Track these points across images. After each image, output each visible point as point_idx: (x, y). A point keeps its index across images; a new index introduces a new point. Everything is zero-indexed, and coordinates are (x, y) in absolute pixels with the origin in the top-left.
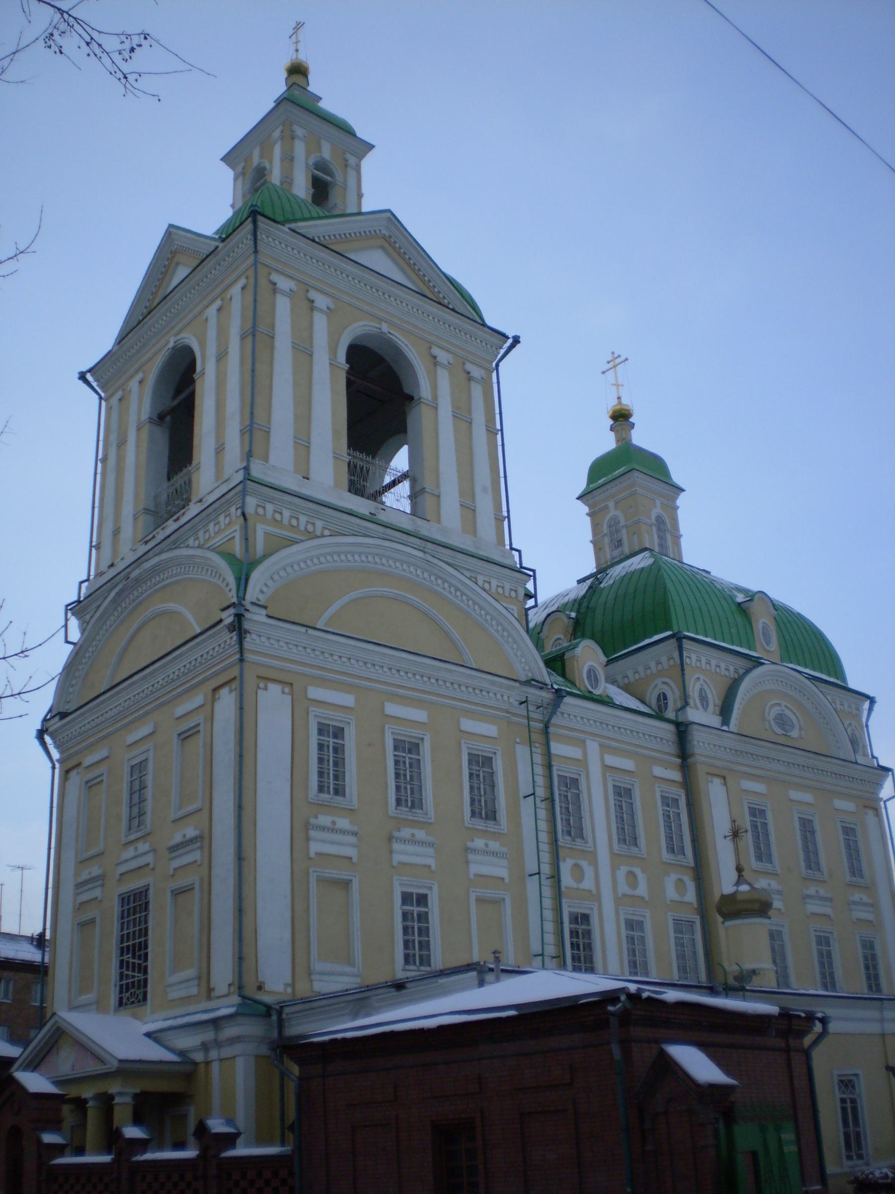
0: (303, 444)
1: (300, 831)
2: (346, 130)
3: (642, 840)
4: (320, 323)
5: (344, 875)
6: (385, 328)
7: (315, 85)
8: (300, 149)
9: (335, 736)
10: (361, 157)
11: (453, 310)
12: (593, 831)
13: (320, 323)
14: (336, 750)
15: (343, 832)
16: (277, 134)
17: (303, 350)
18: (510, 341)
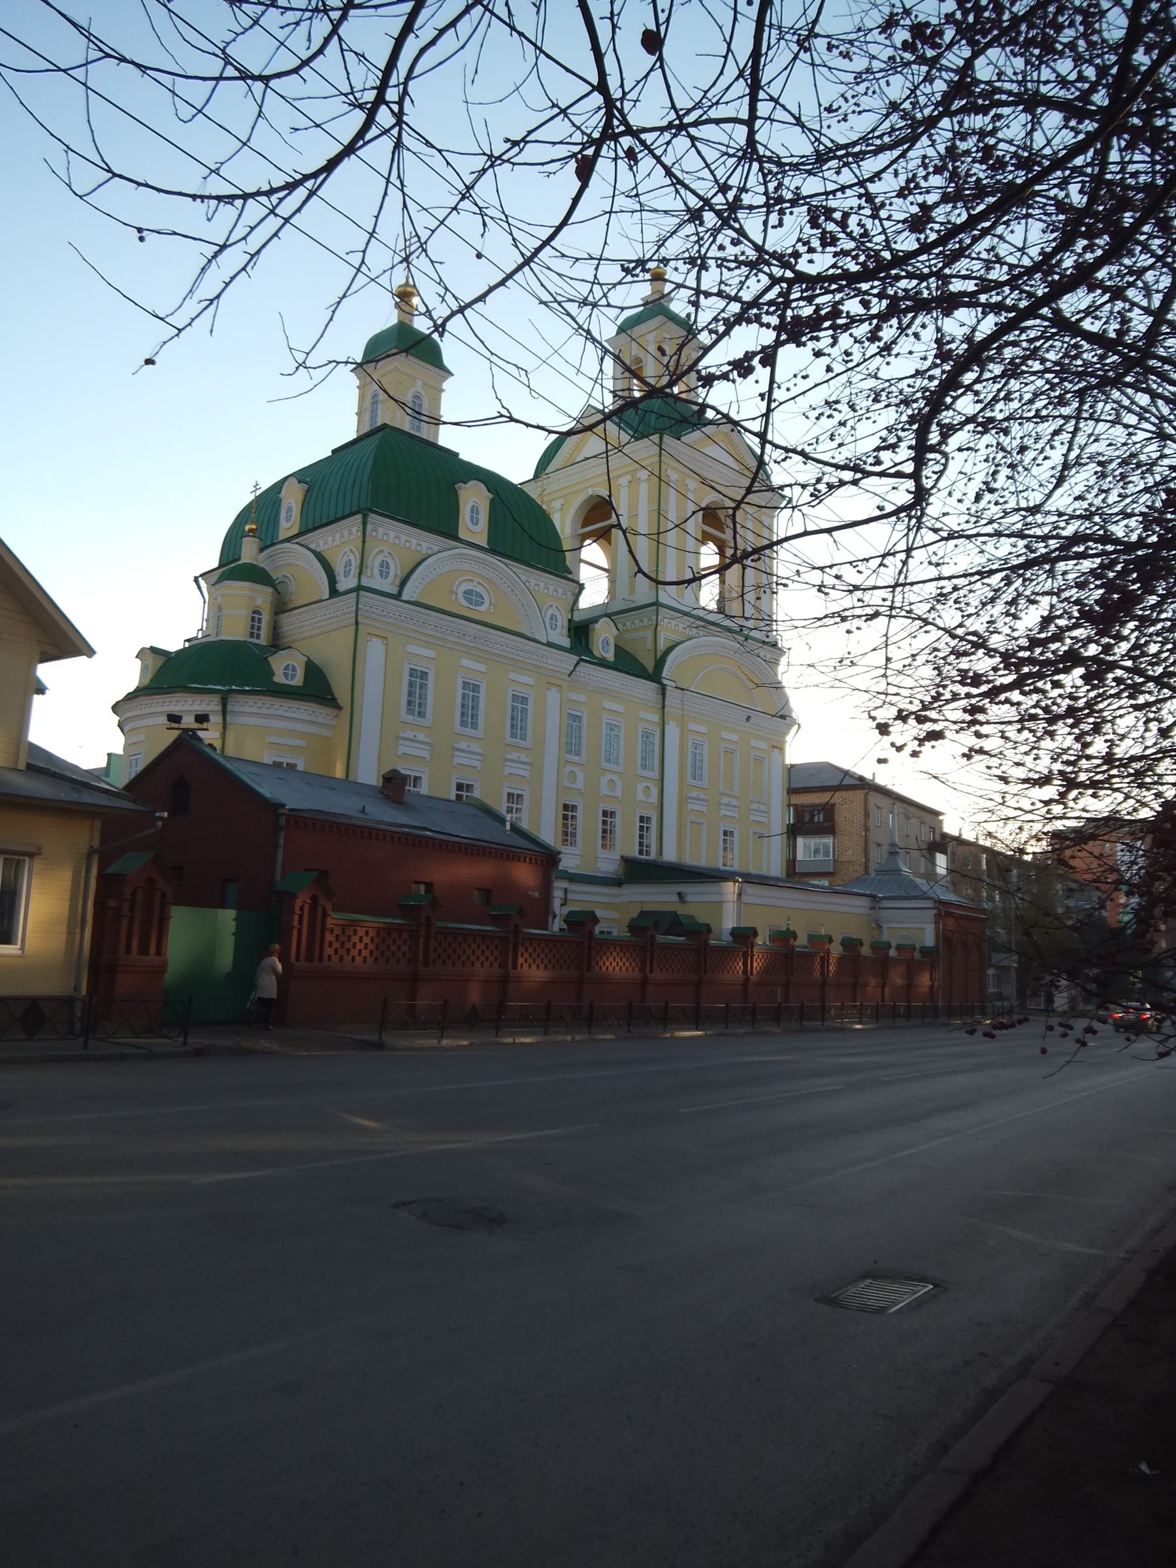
1: (683, 799)
15: (472, 753)
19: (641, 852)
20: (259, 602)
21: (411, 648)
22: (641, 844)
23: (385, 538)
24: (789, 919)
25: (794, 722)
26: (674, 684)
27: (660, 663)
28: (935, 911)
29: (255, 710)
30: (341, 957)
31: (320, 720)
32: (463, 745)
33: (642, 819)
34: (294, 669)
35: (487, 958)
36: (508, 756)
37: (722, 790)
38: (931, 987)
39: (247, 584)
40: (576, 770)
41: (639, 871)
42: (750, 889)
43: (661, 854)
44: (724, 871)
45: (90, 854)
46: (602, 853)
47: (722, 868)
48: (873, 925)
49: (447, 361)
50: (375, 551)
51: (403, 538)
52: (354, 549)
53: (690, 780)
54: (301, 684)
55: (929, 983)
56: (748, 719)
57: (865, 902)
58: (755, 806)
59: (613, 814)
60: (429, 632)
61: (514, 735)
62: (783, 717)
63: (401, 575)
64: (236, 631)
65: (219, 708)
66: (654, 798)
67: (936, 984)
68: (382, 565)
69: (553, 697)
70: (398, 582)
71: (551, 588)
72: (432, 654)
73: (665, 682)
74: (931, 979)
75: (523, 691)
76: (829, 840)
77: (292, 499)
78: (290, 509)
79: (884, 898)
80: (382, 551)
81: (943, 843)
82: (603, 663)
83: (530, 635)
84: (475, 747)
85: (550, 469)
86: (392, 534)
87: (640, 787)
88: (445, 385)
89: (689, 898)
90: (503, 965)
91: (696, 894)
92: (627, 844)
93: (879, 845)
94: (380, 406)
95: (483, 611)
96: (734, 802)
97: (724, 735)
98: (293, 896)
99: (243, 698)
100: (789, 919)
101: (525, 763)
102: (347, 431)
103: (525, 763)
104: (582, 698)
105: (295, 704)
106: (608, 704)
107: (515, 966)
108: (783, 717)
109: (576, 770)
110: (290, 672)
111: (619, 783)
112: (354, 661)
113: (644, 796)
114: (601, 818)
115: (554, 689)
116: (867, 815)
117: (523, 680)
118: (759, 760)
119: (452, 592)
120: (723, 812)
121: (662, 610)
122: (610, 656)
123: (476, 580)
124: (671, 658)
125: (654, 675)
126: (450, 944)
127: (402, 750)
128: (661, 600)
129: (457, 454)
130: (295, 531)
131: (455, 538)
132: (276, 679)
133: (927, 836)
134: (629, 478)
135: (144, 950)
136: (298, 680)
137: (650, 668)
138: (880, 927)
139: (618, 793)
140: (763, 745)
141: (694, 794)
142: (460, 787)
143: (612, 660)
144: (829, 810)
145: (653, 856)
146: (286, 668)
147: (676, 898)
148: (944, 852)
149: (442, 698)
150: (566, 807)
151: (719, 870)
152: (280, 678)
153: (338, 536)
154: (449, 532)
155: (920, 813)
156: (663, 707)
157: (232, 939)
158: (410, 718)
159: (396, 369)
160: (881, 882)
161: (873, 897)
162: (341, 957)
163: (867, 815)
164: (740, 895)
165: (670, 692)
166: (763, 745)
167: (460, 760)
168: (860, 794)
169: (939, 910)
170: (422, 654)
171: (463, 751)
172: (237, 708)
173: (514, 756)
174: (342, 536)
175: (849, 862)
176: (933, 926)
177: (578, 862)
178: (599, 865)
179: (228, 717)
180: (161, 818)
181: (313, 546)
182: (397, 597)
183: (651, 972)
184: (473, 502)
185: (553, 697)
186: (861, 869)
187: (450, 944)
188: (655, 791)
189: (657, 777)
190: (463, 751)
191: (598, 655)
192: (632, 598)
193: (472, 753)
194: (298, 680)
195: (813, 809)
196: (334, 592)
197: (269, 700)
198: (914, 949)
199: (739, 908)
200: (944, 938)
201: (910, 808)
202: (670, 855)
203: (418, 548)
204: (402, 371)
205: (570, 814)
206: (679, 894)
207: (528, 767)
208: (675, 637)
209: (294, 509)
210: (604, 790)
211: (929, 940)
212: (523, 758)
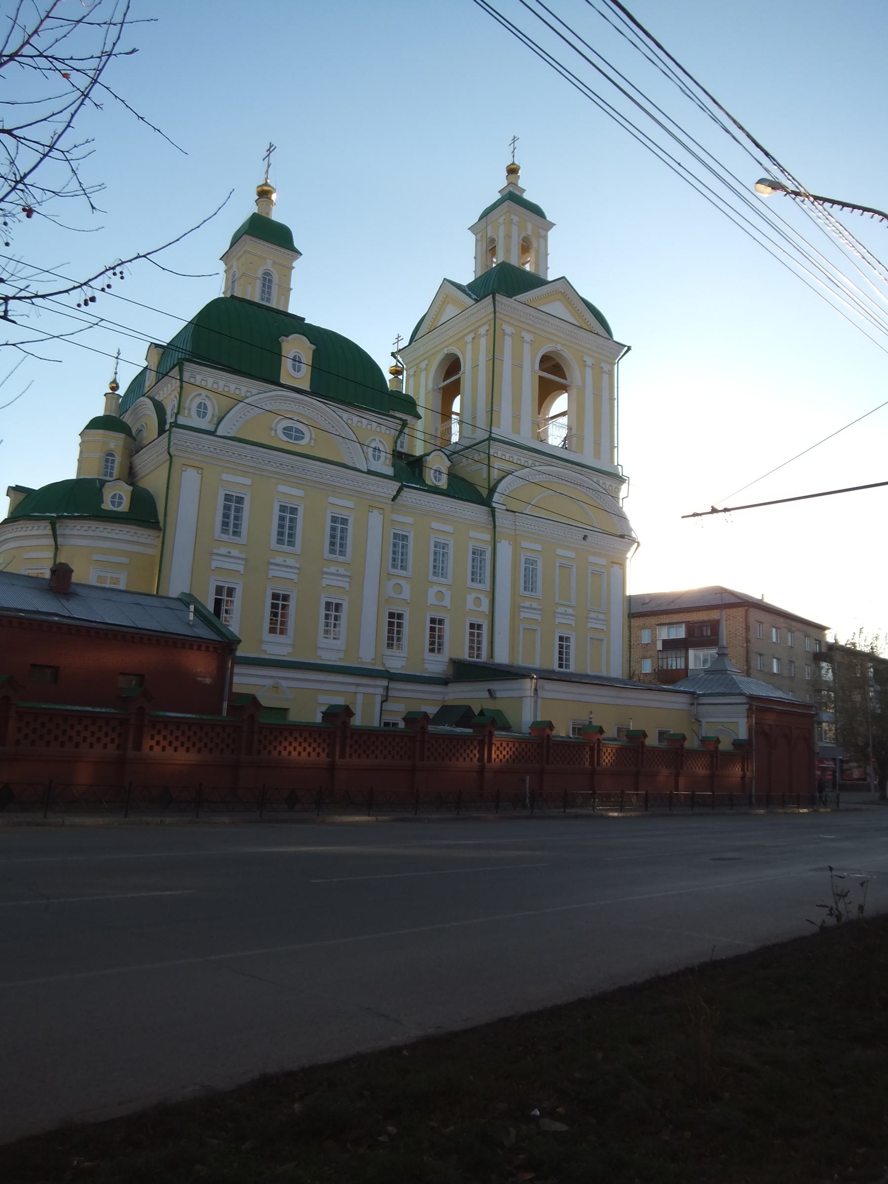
0: (516, 418)
1: (516, 609)
2: (536, 211)
3: (539, 584)
4: (527, 348)
5: (534, 627)
6: (559, 347)
7: (524, 181)
8: (515, 229)
9: (443, 548)
10: (547, 231)
11: (597, 334)
12: (165, 515)
13: (527, 348)
14: (443, 555)
15: (534, 609)
16: (501, 220)
17: (518, 366)
18: (626, 348)
19: (561, 666)
20: (112, 446)
21: (224, 476)
22: (561, 659)
25: (634, 541)
26: (504, 508)
27: (492, 491)
28: (747, 706)
29: (82, 533)
30: (318, 754)
31: (142, 540)
32: (279, 560)
33: (472, 626)
34: (121, 497)
35: (305, 749)
36: (326, 570)
37: (557, 600)
39: (101, 432)
40: (402, 582)
41: (463, 671)
42: (548, 685)
43: (492, 657)
46: (428, 656)
48: (693, 720)
51: (222, 383)
53: (522, 592)
54: (127, 510)
55: (740, 773)
56: (585, 538)
57: (684, 699)
58: (593, 615)
59: (441, 622)
60: (247, 463)
61: (332, 551)
64: (92, 474)
65: (51, 532)
66: (485, 607)
67: (748, 774)
68: (199, 406)
69: (375, 518)
70: (215, 420)
72: (248, 481)
73: (494, 505)
74: (743, 770)
75: (342, 514)
76: (713, 651)
79: (703, 695)
80: (200, 394)
82: (435, 490)
83: (351, 465)
84: (291, 562)
87: (470, 598)
88: (295, 264)
89: (498, 695)
91: (504, 689)
92: (457, 646)
93: (761, 655)
95: (303, 445)
96: (570, 611)
97: (560, 552)
99: (71, 523)
104: (409, 520)
105: (117, 527)
106: (435, 525)
107: (138, 746)
109: (402, 582)
110: (117, 500)
111: (447, 594)
112: (168, 488)
113: (474, 605)
114: (468, 630)
116: (747, 629)
117: (343, 505)
119: (271, 429)
120: (558, 620)
122: (443, 483)
125: (485, 501)
126: (454, 746)
127: (214, 564)
129: (304, 319)
132: (104, 506)
133: (810, 646)
134: (472, 335)
136: (124, 507)
138: (699, 721)
139: (447, 602)
143: (445, 487)
144: (715, 626)
145: (484, 658)
146: (114, 497)
147: (486, 695)
149: (312, 531)
150: (391, 615)
151: (553, 672)
152: (107, 505)
155: (781, 621)
156: (495, 527)
158: (225, 537)
159: (246, 252)
161: (693, 694)
162: (318, 754)
163: (747, 629)
164: (536, 690)
166: (603, 561)
167: (219, 565)
168: (741, 611)
169: (751, 705)
170: (238, 482)
171: (278, 565)
172: (67, 532)
173: (333, 569)
176: (745, 720)
177: (404, 663)
178: (426, 666)
179: (59, 540)
182: (212, 433)
183: (342, 756)
184: (295, 348)
185: (375, 518)
187: (454, 746)
189: (487, 586)
190: (278, 565)
192: (473, 436)
193: (534, 609)
194: (124, 507)
195: (702, 624)
197: (93, 524)
199: (536, 702)
200: (759, 731)
201: (794, 624)
202: (502, 657)
203: (237, 392)
204: (264, 253)
205: (564, 643)
206: (489, 690)
207: (348, 580)
210: (432, 599)
212: (342, 571)
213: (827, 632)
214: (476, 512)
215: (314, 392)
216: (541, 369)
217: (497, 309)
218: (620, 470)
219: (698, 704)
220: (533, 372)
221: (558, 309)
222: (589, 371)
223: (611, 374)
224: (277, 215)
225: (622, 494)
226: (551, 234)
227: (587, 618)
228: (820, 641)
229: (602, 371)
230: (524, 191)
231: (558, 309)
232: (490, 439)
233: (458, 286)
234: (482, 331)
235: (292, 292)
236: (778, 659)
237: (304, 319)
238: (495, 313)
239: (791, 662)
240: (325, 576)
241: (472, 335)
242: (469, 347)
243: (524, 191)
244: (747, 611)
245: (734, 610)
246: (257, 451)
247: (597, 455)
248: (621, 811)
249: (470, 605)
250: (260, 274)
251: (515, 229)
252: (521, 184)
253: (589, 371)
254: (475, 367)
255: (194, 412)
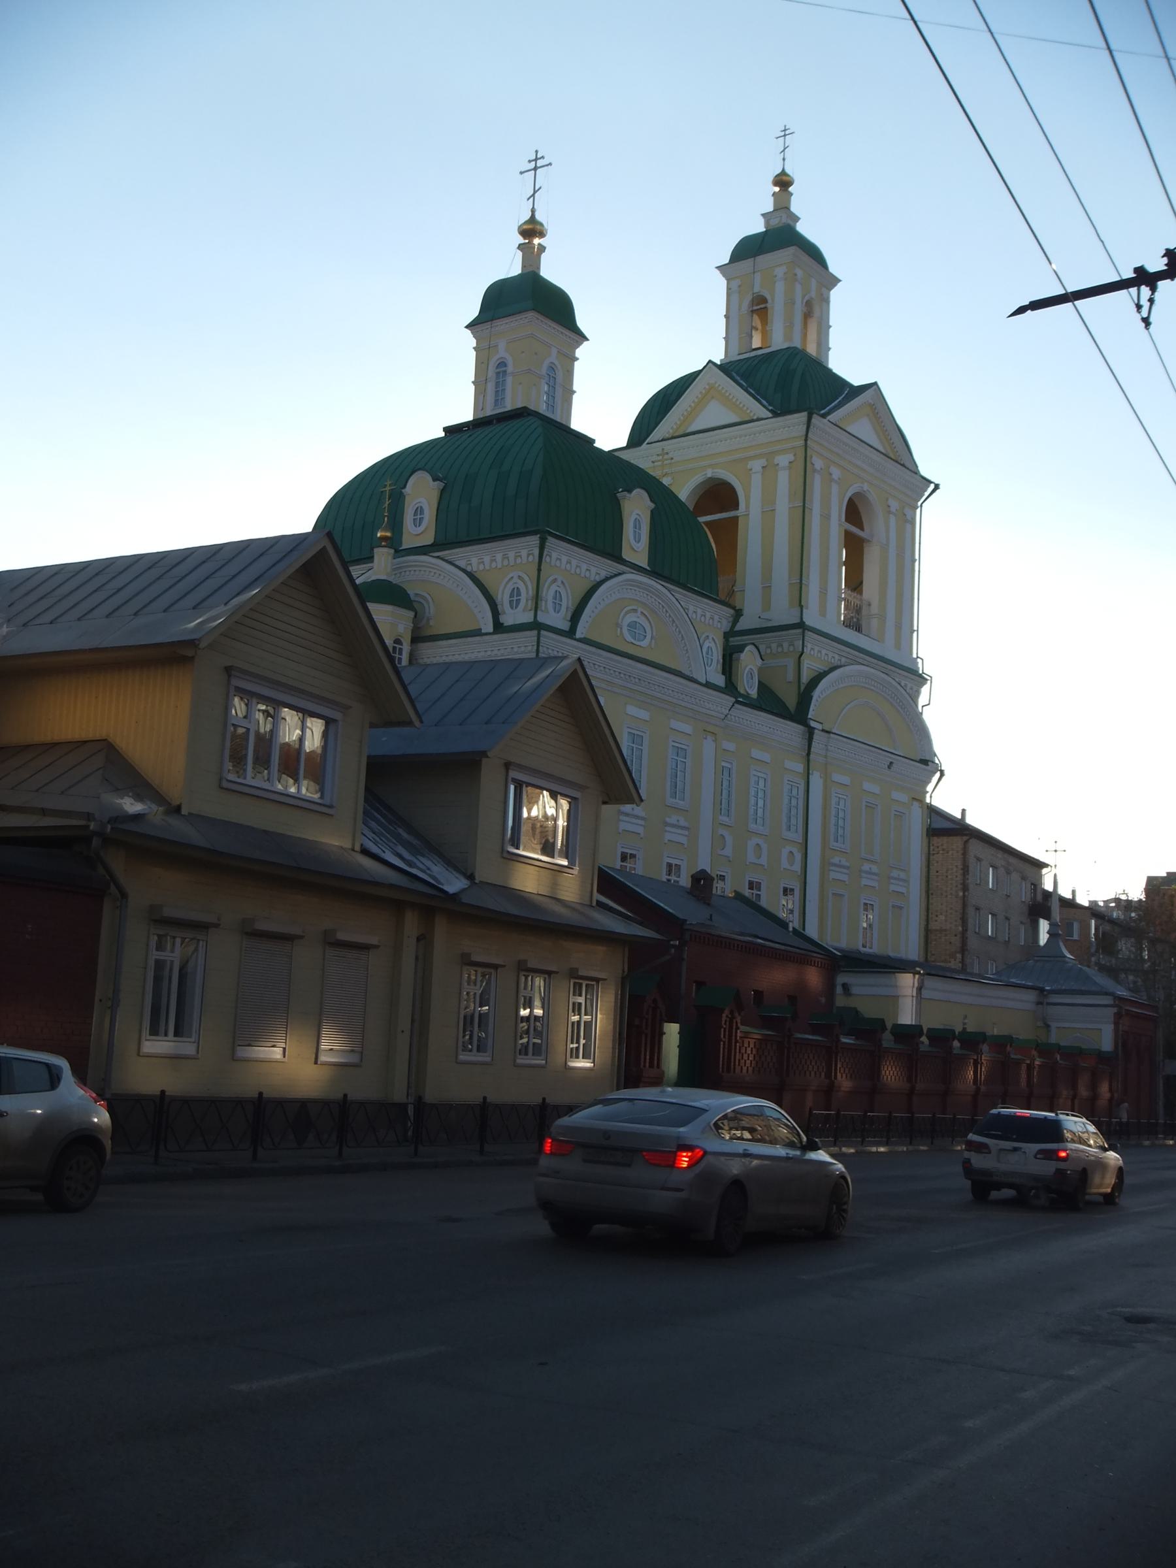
1: (825, 865)
2: (814, 254)
4: (835, 489)
8: (798, 289)
11: (903, 465)
13: (835, 489)
18: (932, 487)
19: (864, 946)
23: (578, 571)
24: (965, 1017)
27: (805, 698)
28: (1115, 1010)
38: (1111, 1100)
42: (930, 982)
44: (865, 954)
45: (623, 979)
47: (863, 950)
48: (1040, 1024)
49: (582, 322)
50: (551, 578)
52: (526, 578)
55: (1108, 1095)
57: (1031, 996)
62: (925, 762)
63: (572, 608)
66: (797, 867)
67: (1116, 1095)
69: (708, 747)
71: (708, 615)
73: (813, 724)
74: (1111, 1090)
77: (422, 494)
78: (419, 511)
81: (1043, 904)
83: (687, 673)
85: (657, 434)
86: (564, 559)
87: (785, 853)
88: (579, 352)
90: (828, 1076)
93: (977, 909)
94: (509, 380)
96: (875, 869)
98: (722, 1011)
100: (965, 1017)
101: (683, 828)
102: (461, 408)
103: (683, 828)
106: (756, 753)
108: (925, 762)
115: (710, 738)
118: (900, 816)
120: (864, 882)
121: (808, 634)
122: (754, 693)
123: (640, 610)
124: (816, 694)
125: (799, 714)
128: (808, 621)
129: (593, 441)
130: (429, 539)
131: (619, 559)
134: (763, 462)
135: (651, 1066)
137: (791, 702)
138: (1048, 1026)
139: (764, 860)
140: (903, 797)
141: (836, 860)
142: (624, 857)
148: (1047, 917)
153: (499, 557)
154: (613, 553)
156: (808, 754)
157: (677, 1050)
160: (1036, 972)
161: (1042, 990)
163: (965, 869)
164: (920, 989)
165: (818, 736)
166: (903, 797)
168: (957, 842)
174: (505, 557)
175: (941, 930)
176: (1112, 1026)
180: (674, 946)
181: (462, 564)
182: (571, 633)
185: (708, 747)
186: (956, 941)
188: (798, 857)
191: (742, 692)
196: (499, 627)
198: (884, 1028)
200: (1122, 1039)
201: (1012, 860)
203: (587, 574)
208: (821, 667)
209: (426, 511)
210: (751, 857)
211: (1106, 1043)
213: (1044, 871)
214: (791, 731)
215: (655, 572)
216: (847, 520)
217: (810, 435)
218: (920, 665)
219: (1048, 1004)
220: (840, 525)
221: (864, 429)
222: (892, 519)
223: (912, 523)
224: (550, 271)
225: (922, 700)
226: (835, 295)
227: (667, 824)
228: (1036, 884)
229: (906, 521)
230: (797, 219)
231: (864, 429)
232: (801, 625)
233: (714, 364)
234: (783, 460)
235: (575, 397)
236: (993, 915)
237: (593, 441)
238: (806, 440)
239: (1007, 918)
240: (668, 829)
241: (763, 462)
242: (756, 480)
243: (797, 219)
244: (966, 842)
245: (945, 839)
246: (600, 655)
247: (898, 645)
248: (887, 1144)
249: (785, 864)
250: (544, 371)
251: (798, 289)
252: (794, 208)
253: (892, 519)
254: (769, 513)
255: (551, 610)
